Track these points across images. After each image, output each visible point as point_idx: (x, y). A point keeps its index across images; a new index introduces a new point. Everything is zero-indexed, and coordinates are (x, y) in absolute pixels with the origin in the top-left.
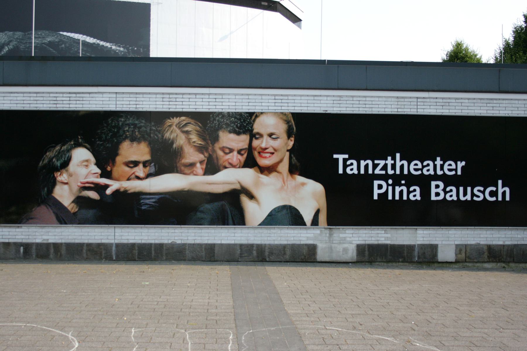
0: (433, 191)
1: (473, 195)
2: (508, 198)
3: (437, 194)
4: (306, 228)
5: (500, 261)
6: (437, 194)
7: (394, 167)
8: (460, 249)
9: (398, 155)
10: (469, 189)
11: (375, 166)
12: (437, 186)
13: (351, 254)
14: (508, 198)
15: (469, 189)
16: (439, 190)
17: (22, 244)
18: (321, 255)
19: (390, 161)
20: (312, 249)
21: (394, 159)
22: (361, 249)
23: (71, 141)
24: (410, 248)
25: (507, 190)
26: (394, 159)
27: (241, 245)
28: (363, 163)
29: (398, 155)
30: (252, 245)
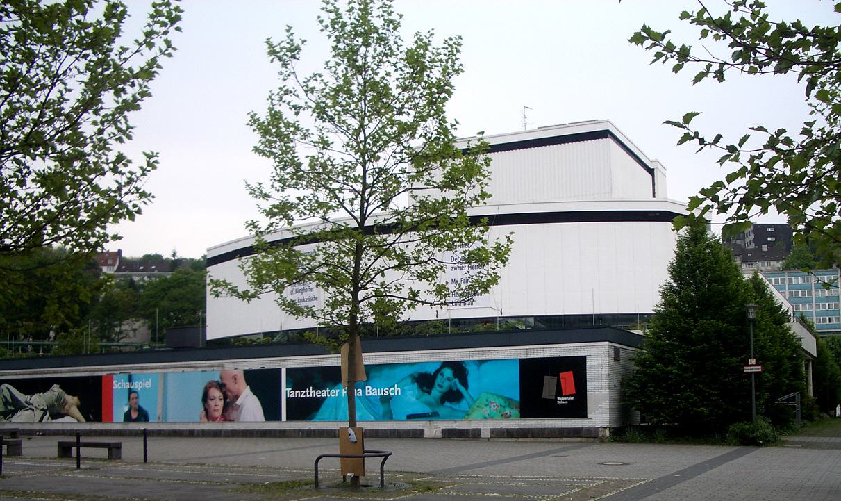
0: (367, 391)
1: (384, 392)
2: (400, 394)
3: (369, 393)
4: (576, 432)
5: (512, 437)
6: (369, 393)
7: (309, 394)
8: (492, 431)
9: (311, 388)
10: (382, 390)
11: (301, 393)
12: (369, 389)
13: (440, 435)
14: (400, 394)
15: (382, 390)
16: (369, 391)
17: (300, 430)
18: (426, 434)
19: (308, 391)
20: (422, 431)
21: (309, 390)
22: (444, 431)
23: (85, 6)
24: (467, 431)
25: (399, 389)
26: (309, 390)
27: (390, 430)
28: (297, 392)
29: (311, 388)
30: (395, 430)
